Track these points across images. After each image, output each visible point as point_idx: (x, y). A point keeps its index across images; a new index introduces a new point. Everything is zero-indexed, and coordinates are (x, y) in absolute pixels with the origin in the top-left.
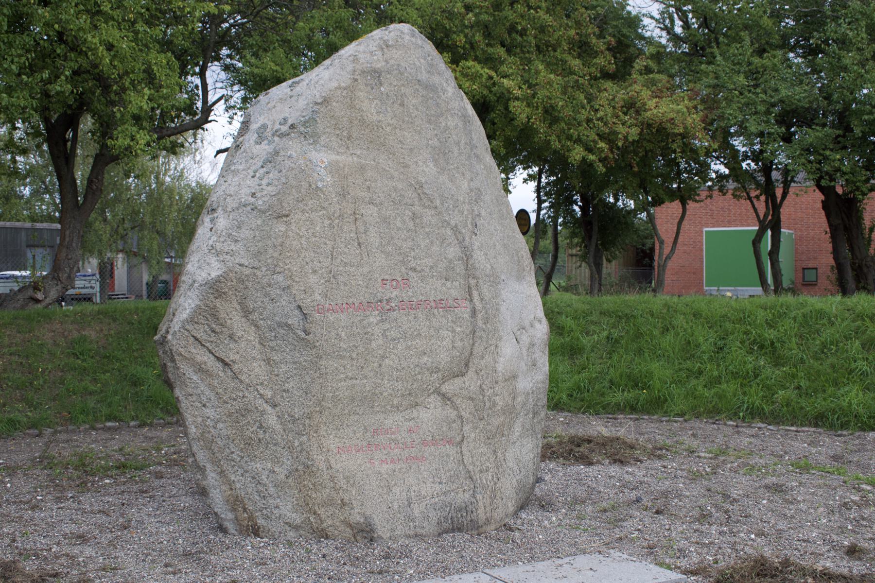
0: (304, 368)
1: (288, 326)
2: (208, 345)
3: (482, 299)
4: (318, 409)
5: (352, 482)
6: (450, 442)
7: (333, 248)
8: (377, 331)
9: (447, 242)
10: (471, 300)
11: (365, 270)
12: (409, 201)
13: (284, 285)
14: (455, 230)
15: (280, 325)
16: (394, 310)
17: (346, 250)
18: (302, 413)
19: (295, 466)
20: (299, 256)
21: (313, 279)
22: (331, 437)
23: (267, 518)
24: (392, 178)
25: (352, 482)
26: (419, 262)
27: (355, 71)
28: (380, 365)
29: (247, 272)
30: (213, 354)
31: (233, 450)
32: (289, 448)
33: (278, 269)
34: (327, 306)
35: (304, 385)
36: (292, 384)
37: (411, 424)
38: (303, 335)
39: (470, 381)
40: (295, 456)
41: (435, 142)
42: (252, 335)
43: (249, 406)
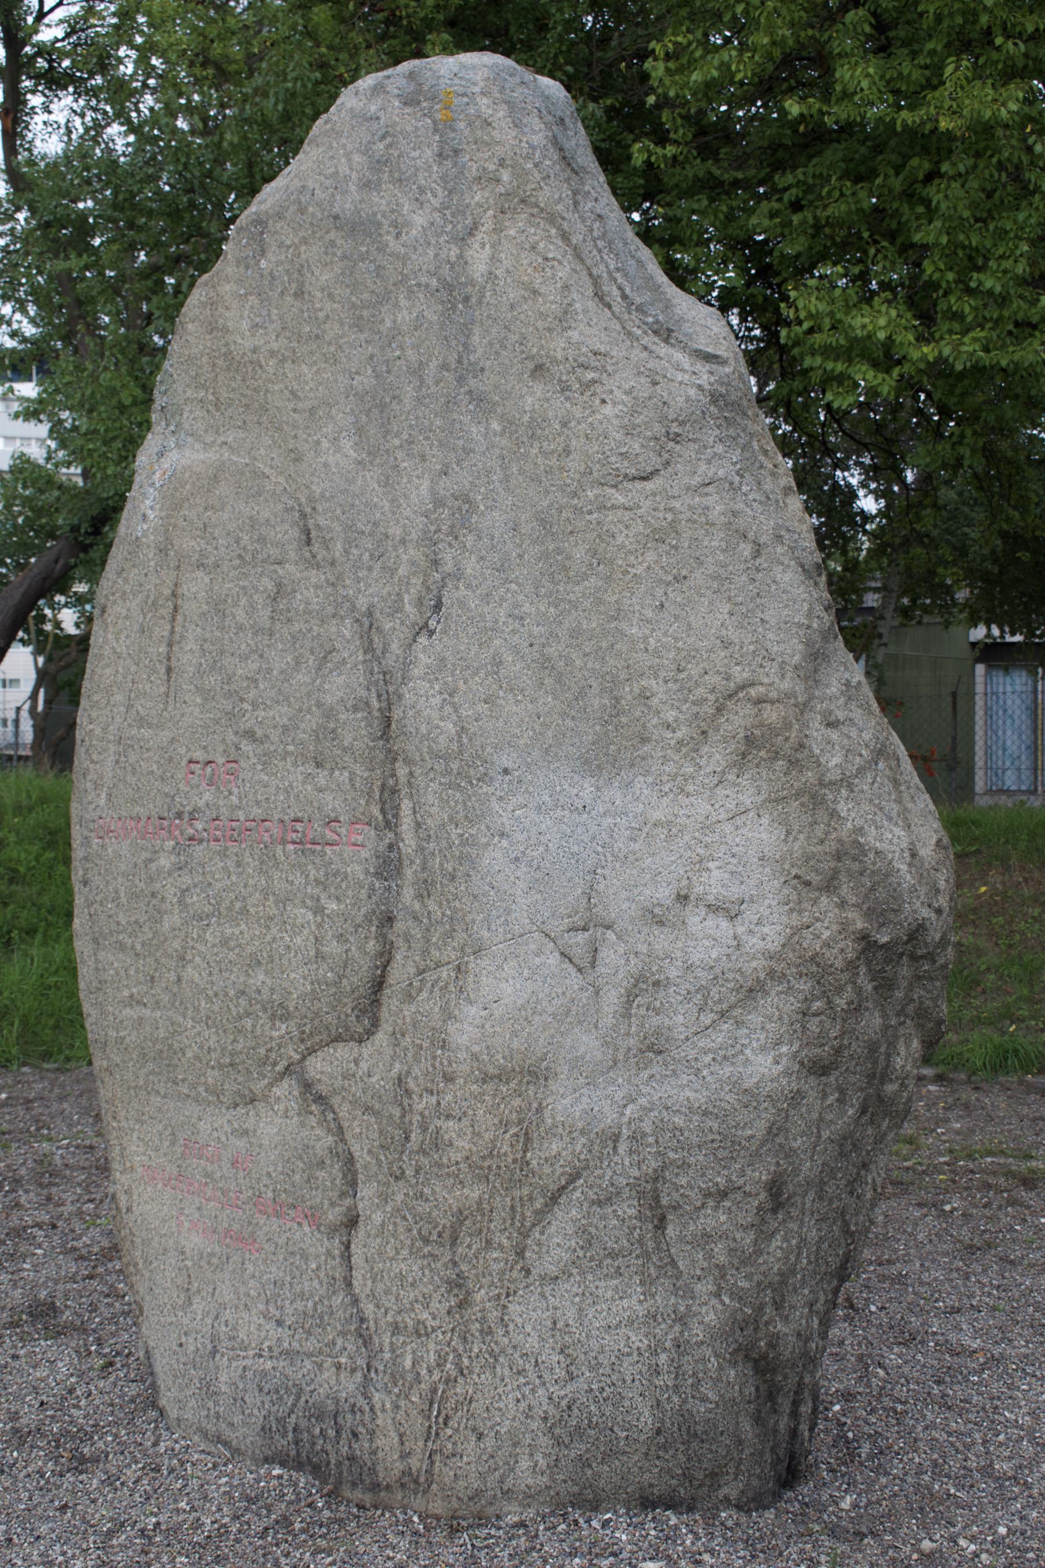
3: (418, 825)
6: (313, 1216)
9: (336, 657)
12: (274, 552)
14: (368, 626)
39: (373, 1062)
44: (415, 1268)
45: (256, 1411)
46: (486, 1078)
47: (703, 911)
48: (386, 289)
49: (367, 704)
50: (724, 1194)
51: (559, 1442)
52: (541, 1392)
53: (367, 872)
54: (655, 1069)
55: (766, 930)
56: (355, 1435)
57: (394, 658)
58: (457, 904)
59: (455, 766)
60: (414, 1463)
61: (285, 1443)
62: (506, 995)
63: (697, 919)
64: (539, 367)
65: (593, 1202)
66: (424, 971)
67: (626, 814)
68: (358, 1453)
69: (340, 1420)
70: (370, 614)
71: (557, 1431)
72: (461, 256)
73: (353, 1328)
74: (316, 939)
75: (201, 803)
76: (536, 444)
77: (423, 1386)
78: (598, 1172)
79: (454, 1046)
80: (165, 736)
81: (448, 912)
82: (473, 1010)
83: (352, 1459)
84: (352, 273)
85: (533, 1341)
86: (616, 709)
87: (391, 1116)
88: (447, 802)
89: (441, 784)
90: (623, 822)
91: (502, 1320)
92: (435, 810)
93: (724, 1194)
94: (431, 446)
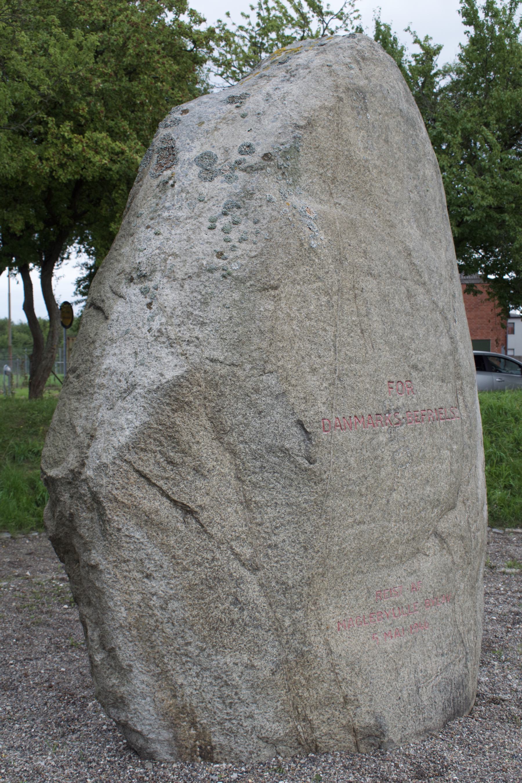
0: (303, 512)
1: (285, 451)
2: (160, 483)
5: (357, 670)
7: (335, 336)
11: (370, 368)
13: (277, 390)
15: (270, 450)
18: (298, 578)
21: (312, 381)
22: (331, 608)
23: (229, 733)
25: (357, 670)
27: (337, 87)
28: (388, 501)
29: (224, 370)
30: (168, 497)
31: (190, 640)
32: (276, 630)
33: (269, 367)
35: (302, 538)
36: (282, 536)
38: (306, 464)
40: (284, 641)
42: (226, 466)
43: (221, 574)
75: (400, 404)
80: (370, 368)
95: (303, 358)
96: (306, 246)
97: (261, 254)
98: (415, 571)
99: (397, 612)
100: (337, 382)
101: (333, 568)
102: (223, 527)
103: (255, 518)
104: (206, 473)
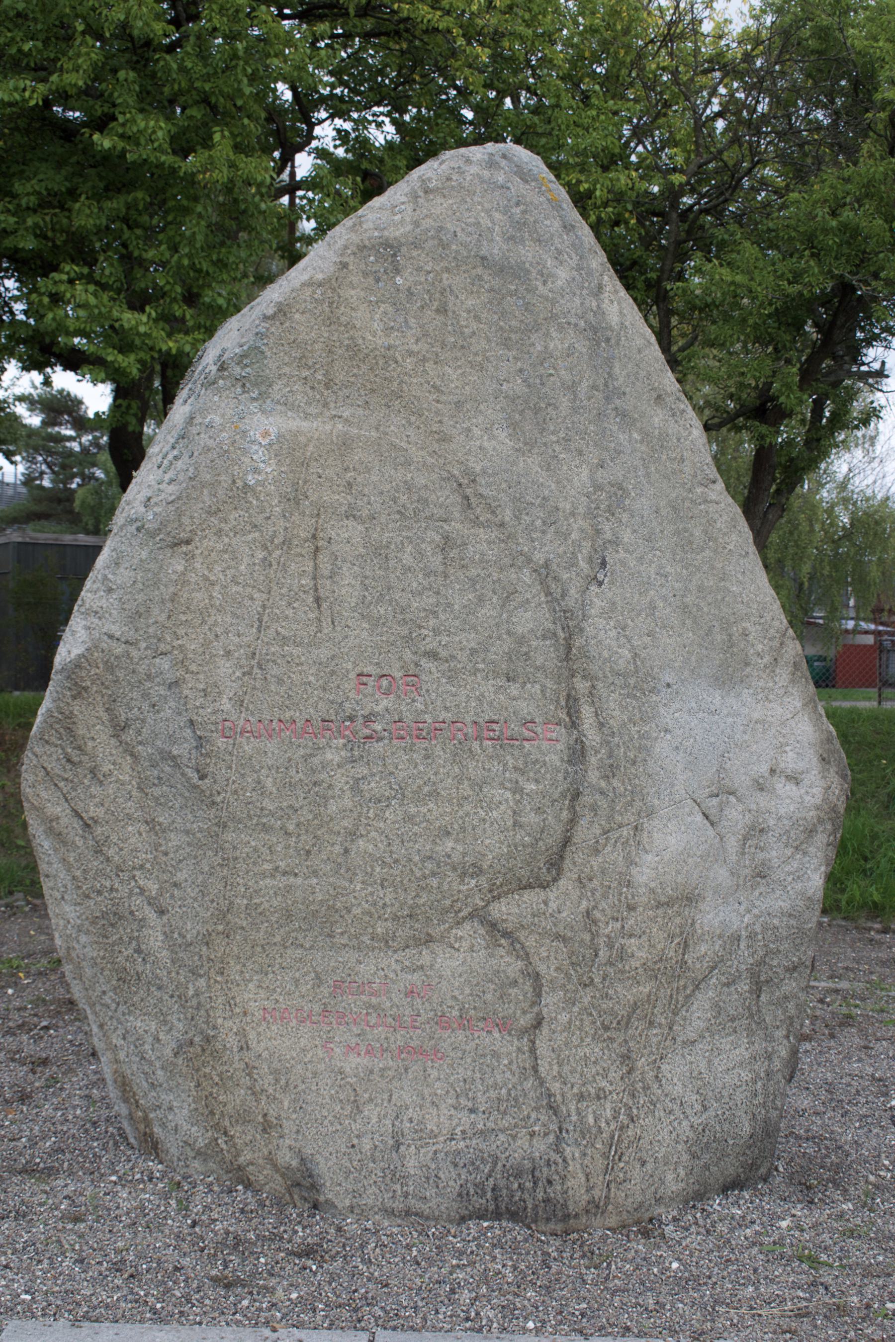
3: (602, 725)
4: (220, 928)
5: (283, 1082)
6: (504, 1026)
7: (264, 607)
8: (340, 780)
9: (519, 599)
10: (574, 725)
11: (323, 653)
12: (438, 512)
13: (170, 677)
14: (545, 574)
16: (380, 739)
17: (290, 612)
19: (190, 1035)
20: (204, 622)
21: (225, 668)
22: (251, 986)
23: (163, 1125)
24: (408, 463)
26: (445, 640)
28: (346, 851)
29: (119, 649)
33: (162, 647)
34: (242, 722)
37: (416, 978)
39: (563, 901)
40: (189, 1016)
41: (517, 386)
44: (597, 1050)
45: (452, 1183)
46: (659, 905)
47: (783, 780)
48: (536, 321)
49: (555, 634)
50: (795, 968)
51: (694, 1156)
52: (685, 1123)
53: (562, 760)
54: (762, 889)
55: (814, 790)
56: (550, 1182)
57: (573, 600)
58: (637, 781)
59: (632, 681)
60: (596, 1193)
61: (484, 1201)
62: (671, 844)
63: (781, 785)
64: (659, 397)
65: (725, 985)
66: (609, 831)
67: (739, 715)
68: (552, 1195)
69: (537, 1174)
70: (547, 565)
71: (694, 1148)
72: (598, 307)
73: (544, 1103)
74: (515, 812)
76: (665, 452)
77: (604, 1135)
78: (729, 963)
79: (636, 884)
81: (629, 788)
82: (649, 857)
83: (547, 1201)
84: (499, 303)
85: (679, 1088)
86: (731, 644)
87: (582, 941)
88: (626, 707)
89: (620, 694)
90: (739, 720)
91: (657, 1077)
92: (616, 713)
93: (795, 968)
94: (588, 445)
95: (217, 636)
96: (240, 483)
97: (179, 498)
98: (422, 967)
99: (373, 1020)
100: (256, 670)
101: (243, 928)
102: (121, 849)
103: (161, 845)
104: (102, 778)
